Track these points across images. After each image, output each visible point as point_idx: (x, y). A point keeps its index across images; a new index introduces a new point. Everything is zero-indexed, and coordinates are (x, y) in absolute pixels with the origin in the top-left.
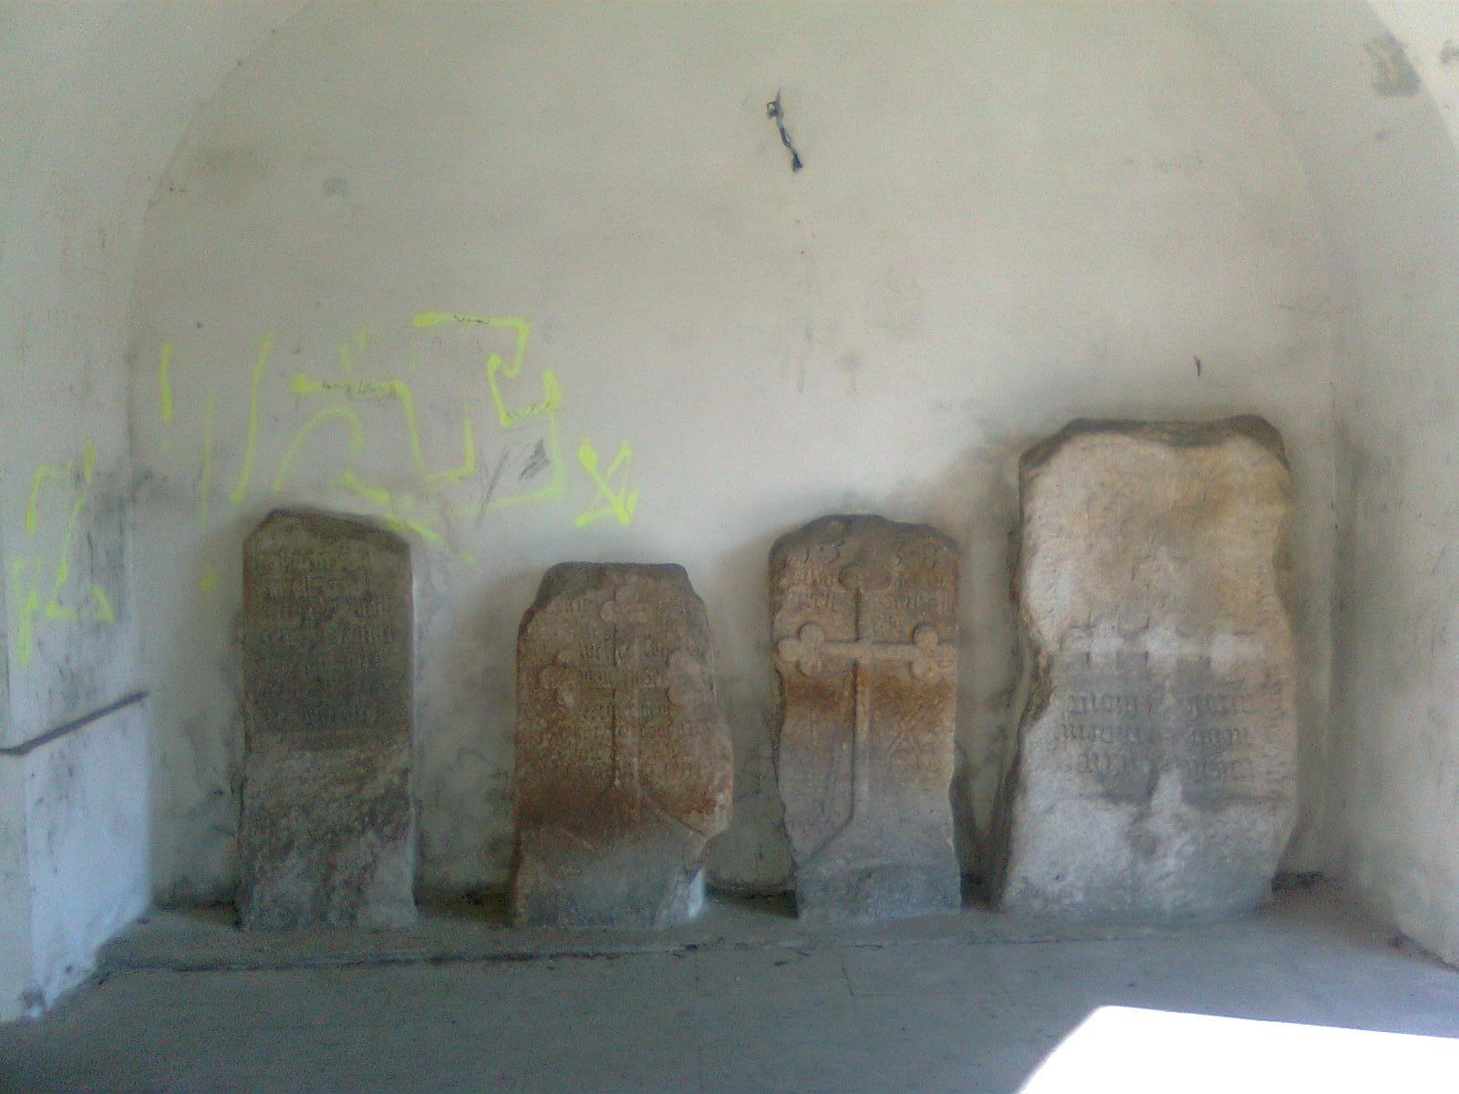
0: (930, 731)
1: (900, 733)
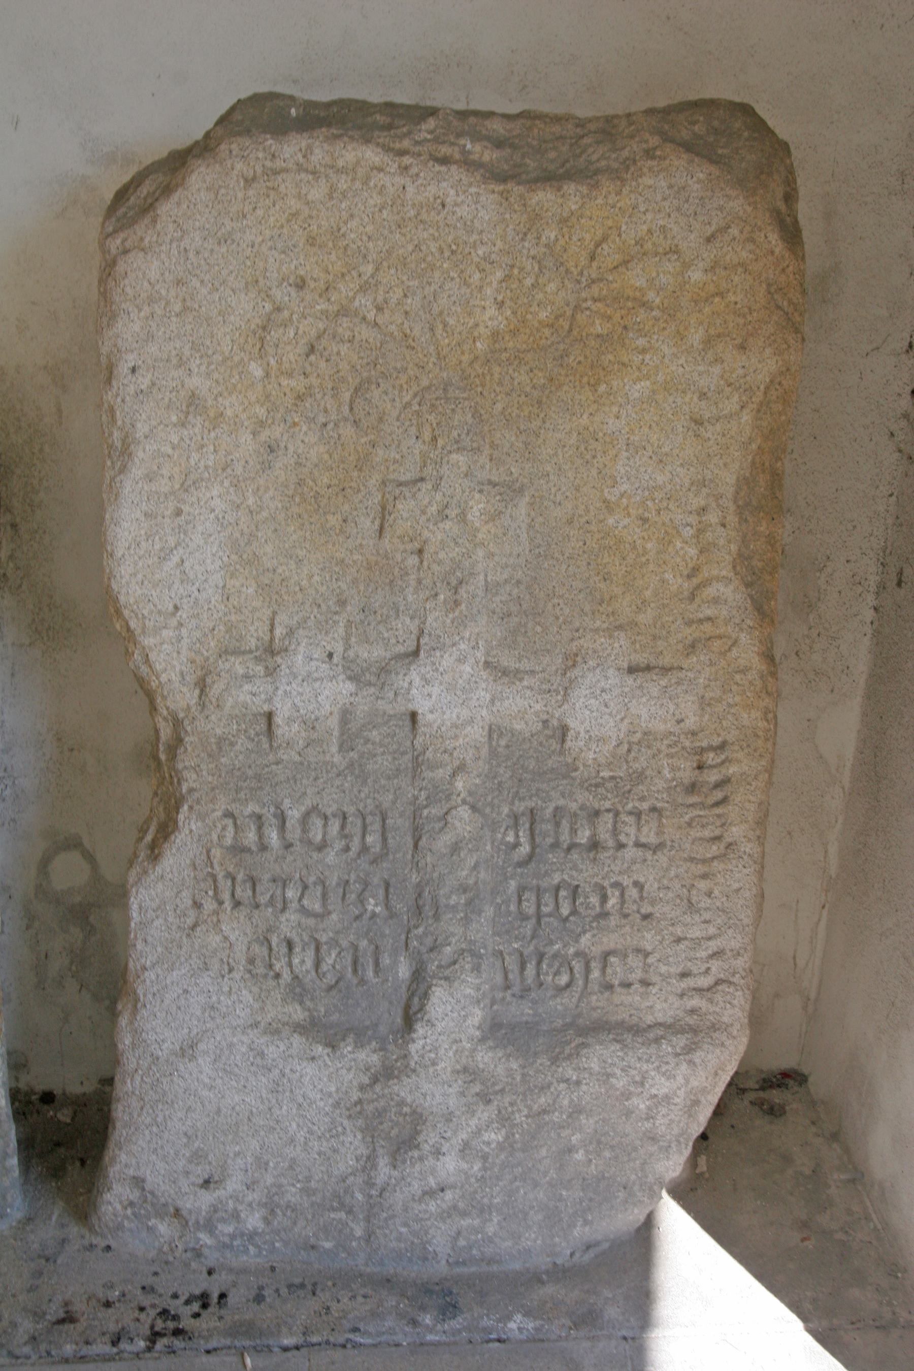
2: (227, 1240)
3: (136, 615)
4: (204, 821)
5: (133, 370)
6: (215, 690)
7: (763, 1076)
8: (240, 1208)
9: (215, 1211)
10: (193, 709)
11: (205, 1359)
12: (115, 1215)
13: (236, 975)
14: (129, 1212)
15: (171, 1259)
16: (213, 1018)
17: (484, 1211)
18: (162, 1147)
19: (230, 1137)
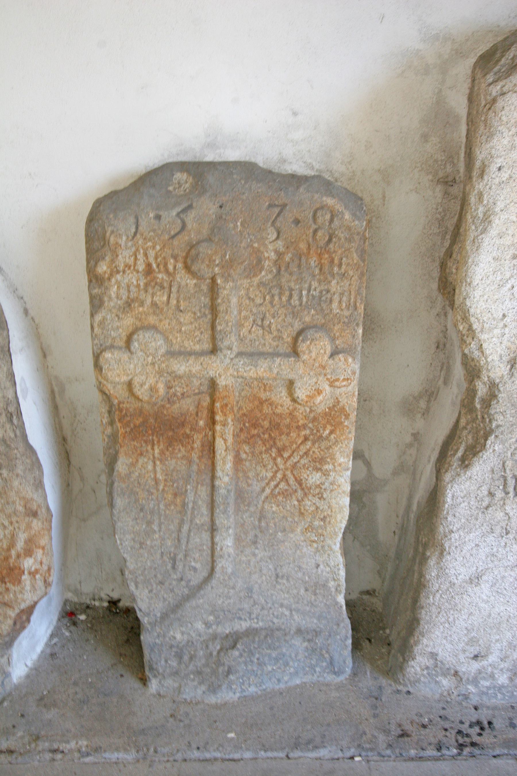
0: (317, 470)
1: (276, 472)
2: (485, 690)
3: (479, 321)
4: (504, 445)
5: (500, 169)
8: (495, 671)
9: (480, 673)
10: (505, 378)
11: (494, 761)
12: (416, 674)
13: (511, 536)
14: (425, 672)
15: (449, 700)
16: (492, 561)
18: (451, 636)
19: (495, 631)
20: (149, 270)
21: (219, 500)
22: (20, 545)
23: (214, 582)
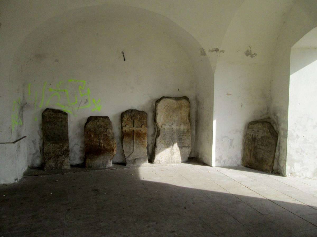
6: (162, 126)
7: (272, 117)
17: (178, 159)
20: (127, 119)
21: (134, 143)
22: (114, 147)
23: (134, 152)
